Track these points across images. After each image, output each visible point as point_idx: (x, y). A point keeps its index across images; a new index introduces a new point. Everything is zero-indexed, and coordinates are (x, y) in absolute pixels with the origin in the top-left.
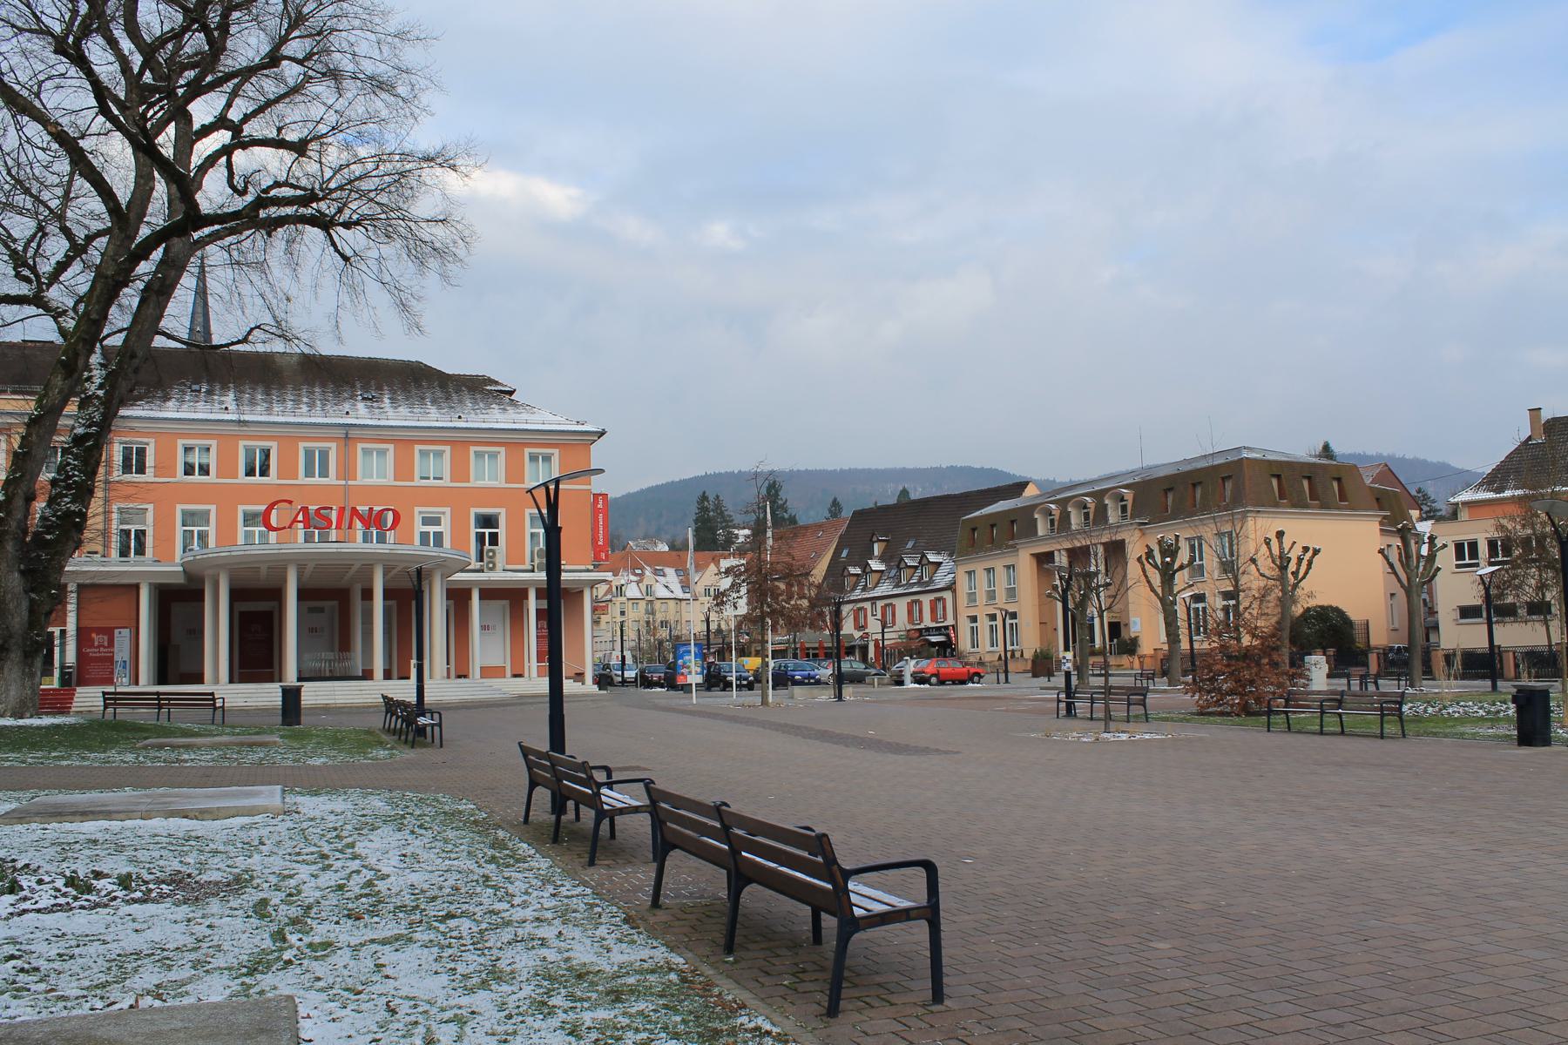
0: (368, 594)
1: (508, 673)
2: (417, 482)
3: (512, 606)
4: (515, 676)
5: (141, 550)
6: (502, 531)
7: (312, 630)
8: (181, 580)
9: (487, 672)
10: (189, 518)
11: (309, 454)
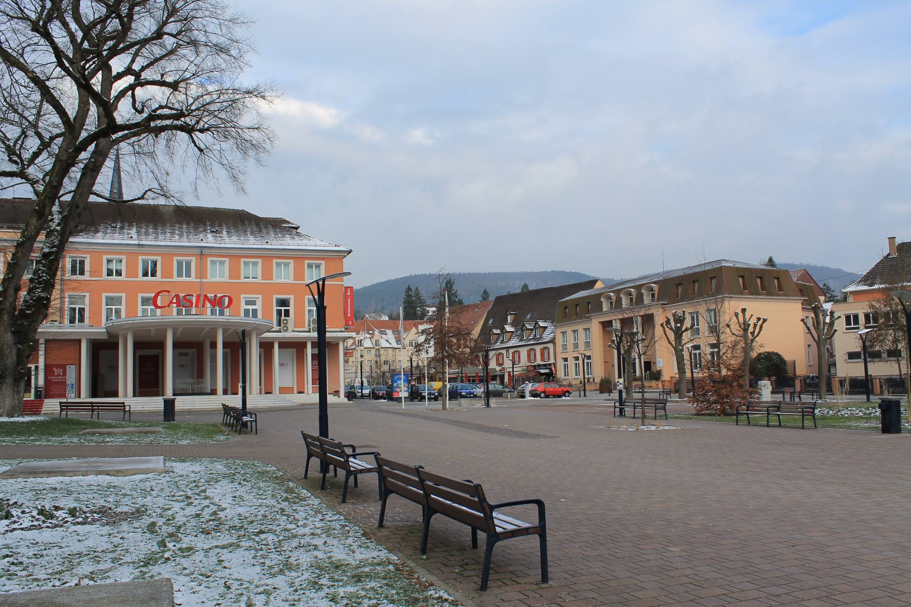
0: (214, 345)
1: (295, 391)
2: (243, 280)
3: (297, 352)
4: (299, 393)
5: (82, 320)
6: (291, 309)
7: (181, 366)
8: (105, 337)
9: (283, 390)
10: (110, 301)
11: (180, 264)
